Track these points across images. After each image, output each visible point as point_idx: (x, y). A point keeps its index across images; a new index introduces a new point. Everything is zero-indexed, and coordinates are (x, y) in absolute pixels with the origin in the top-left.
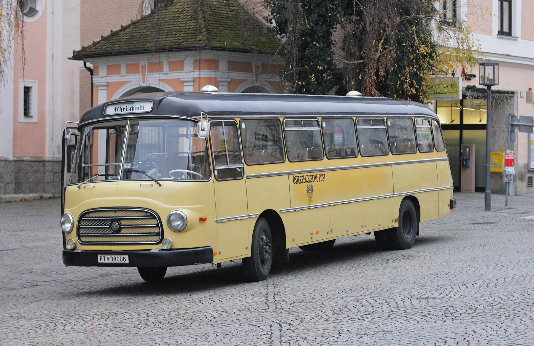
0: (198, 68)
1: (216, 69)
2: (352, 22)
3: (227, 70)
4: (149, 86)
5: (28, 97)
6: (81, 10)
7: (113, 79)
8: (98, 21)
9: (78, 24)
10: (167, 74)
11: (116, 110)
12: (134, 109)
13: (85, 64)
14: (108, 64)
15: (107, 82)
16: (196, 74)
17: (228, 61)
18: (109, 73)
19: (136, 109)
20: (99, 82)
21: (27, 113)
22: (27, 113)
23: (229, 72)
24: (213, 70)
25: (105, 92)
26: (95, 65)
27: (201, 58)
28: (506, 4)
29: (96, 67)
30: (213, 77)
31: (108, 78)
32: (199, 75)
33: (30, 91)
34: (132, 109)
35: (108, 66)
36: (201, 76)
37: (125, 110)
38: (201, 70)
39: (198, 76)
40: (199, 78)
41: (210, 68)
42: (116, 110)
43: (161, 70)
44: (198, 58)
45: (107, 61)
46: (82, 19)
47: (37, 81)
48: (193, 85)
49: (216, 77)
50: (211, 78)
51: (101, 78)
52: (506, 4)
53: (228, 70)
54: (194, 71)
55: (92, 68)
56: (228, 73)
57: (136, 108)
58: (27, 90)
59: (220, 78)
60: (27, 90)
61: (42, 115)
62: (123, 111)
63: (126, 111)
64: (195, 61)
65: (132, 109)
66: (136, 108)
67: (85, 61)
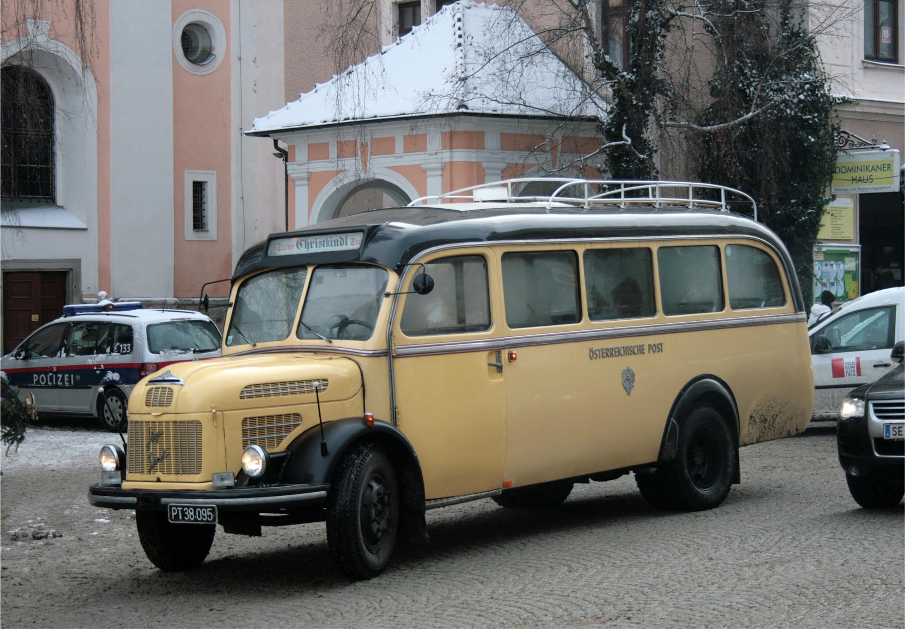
0: (449, 146)
1: (481, 147)
2: (38, 110)
3: (499, 148)
4: (373, 178)
5: (202, 198)
6: (285, 52)
7: (319, 166)
8: (312, 70)
9: (282, 76)
10: (401, 157)
11: (299, 246)
12: (330, 243)
13: (275, 142)
14: (310, 143)
15: (308, 173)
16: (446, 156)
17: (502, 134)
18: (311, 158)
19: (333, 244)
20: (296, 171)
21: (199, 223)
22: (199, 223)
23: (502, 151)
24: (473, 149)
25: (306, 188)
26: (290, 144)
27: (453, 130)
28: (884, 6)
29: (292, 148)
30: (475, 161)
31: (311, 166)
32: (451, 157)
33: (204, 189)
34: (325, 243)
35: (310, 146)
36: (455, 160)
37: (314, 245)
38: (454, 150)
39: (448, 160)
40: (451, 163)
41: (469, 147)
42: (299, 246)
43: (391, 151)
44: (448, 129)
45: (308, 136)
46: (287, 67)
47: (215, 172)
48: (442, 176)
49: (480, 160)
50: (471, 163)
51: (298, 165)
52: (884, 6)
53: (501, 149)
54: (443, 151)
55: (286, 150)
56: (501, 154)
57: (333, 243)
58: (198, 187)
59: (487, 162)
60: (198, 187)
61: (224, 224)
62: (312, 247)
63: (316, 247)
64: (444, 134)
65: (325, 243)
66: (333, 243)
67: (275, 138)
